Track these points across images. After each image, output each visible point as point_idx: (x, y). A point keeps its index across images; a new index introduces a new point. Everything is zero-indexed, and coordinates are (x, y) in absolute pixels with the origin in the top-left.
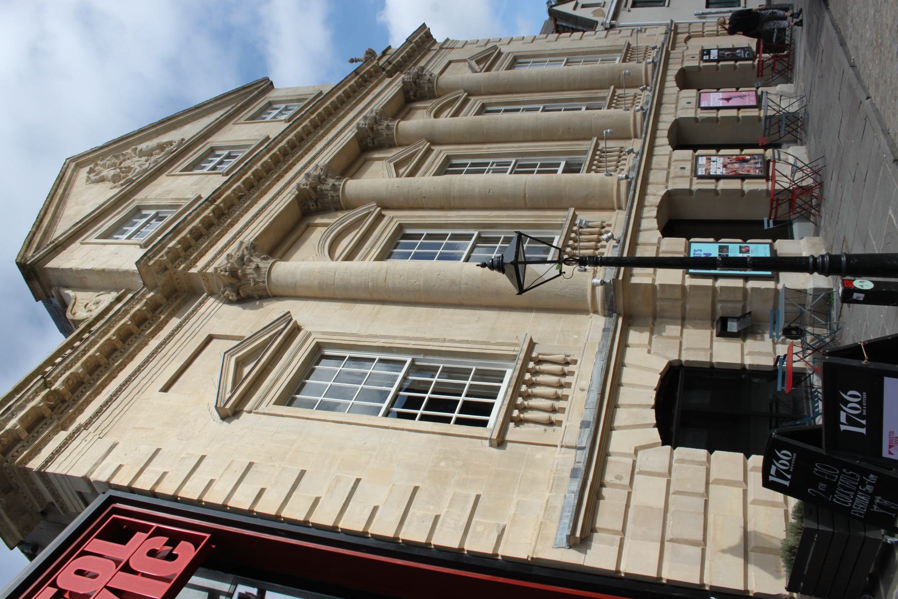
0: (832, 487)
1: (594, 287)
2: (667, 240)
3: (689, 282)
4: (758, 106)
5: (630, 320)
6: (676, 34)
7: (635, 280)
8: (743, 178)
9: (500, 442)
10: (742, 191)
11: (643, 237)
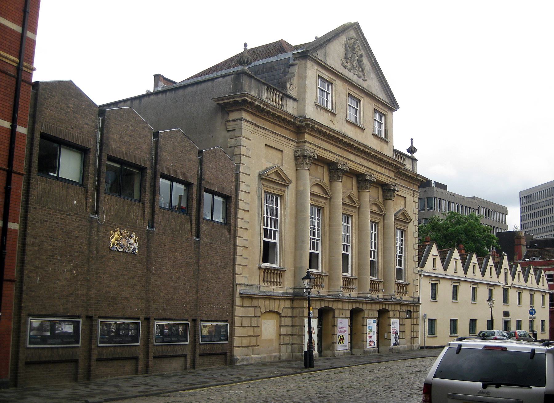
6: (413, 306)
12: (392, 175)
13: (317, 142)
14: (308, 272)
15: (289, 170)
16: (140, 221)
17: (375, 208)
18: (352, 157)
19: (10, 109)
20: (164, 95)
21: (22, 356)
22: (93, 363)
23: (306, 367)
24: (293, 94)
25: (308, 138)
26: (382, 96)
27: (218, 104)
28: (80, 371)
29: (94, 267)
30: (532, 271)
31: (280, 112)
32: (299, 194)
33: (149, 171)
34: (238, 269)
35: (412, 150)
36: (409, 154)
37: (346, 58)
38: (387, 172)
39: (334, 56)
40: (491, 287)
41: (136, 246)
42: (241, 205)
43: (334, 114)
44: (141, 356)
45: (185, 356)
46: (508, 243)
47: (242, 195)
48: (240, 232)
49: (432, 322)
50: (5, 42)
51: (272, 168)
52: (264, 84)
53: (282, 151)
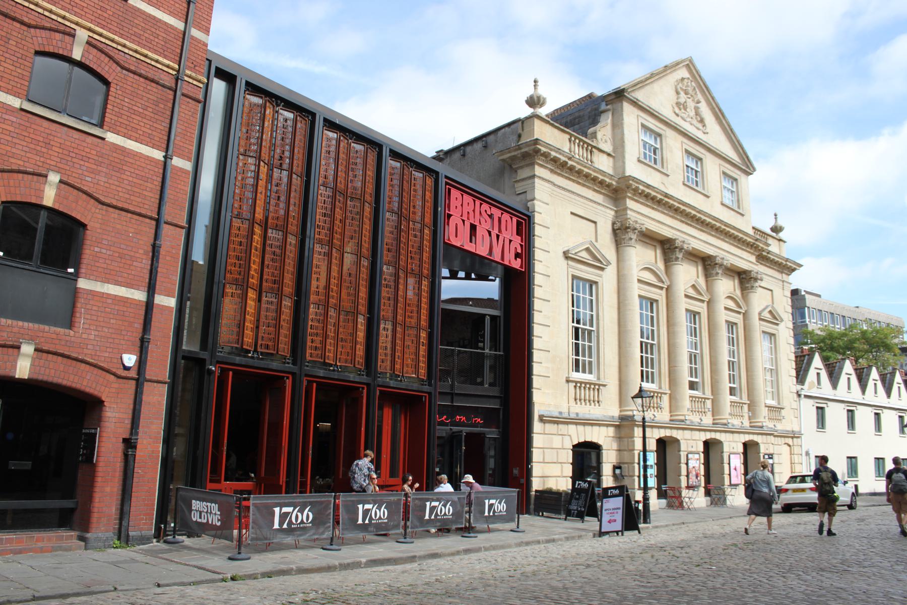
0: (578, 499)
1: (632, 410)
2: (655, 442)
3: (636, 453)
4: (731, 485)
5: (618, 427)
6: (792, 438)
7: (636, 429)
8: (687, 476)
9: (568, 381)
10: (680, 475)
11: (655, 430)
12: (753, 259)
14: (641, 390)
19: (164, 133)
25: (630, 204)
27: (503, 160)
31: (589, 168)
50: (156, 40)
51: (582, 244)
53: (595, 223)
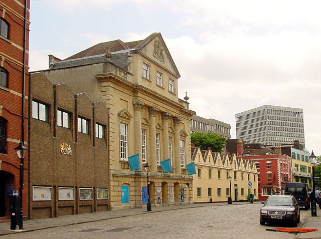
9: (120, 162)
12: (178, 112)
13: (144, 96)
15: (131, 111)
16: (71, 139)
17: (170, 130)
18: (159, 103)
20: (64, 70)
21: (31, 205)
22: (57, 208)
23: (148, 211)
24: (131, 72)
25: (139, 94)
26: (172, 71)
28: (52, 212)
29: (56, 162)
30: (248, 162)
32: (135, 123)
33: (74, 114)
34: (111, 162)
35: (187, 98)
36: (185, 101)
37: (155, 52)
38: (176, 111)
39: (149, 51)
40: (228, 171)
41: (71, 151)
42: (111, 129)
43: (150, 82)
44: (75, 206)
45: (91, 206)
46: (232, 147)
47: (111, 125)
48: (111, 143)
49: (199, 189)
52: (118, 67)
